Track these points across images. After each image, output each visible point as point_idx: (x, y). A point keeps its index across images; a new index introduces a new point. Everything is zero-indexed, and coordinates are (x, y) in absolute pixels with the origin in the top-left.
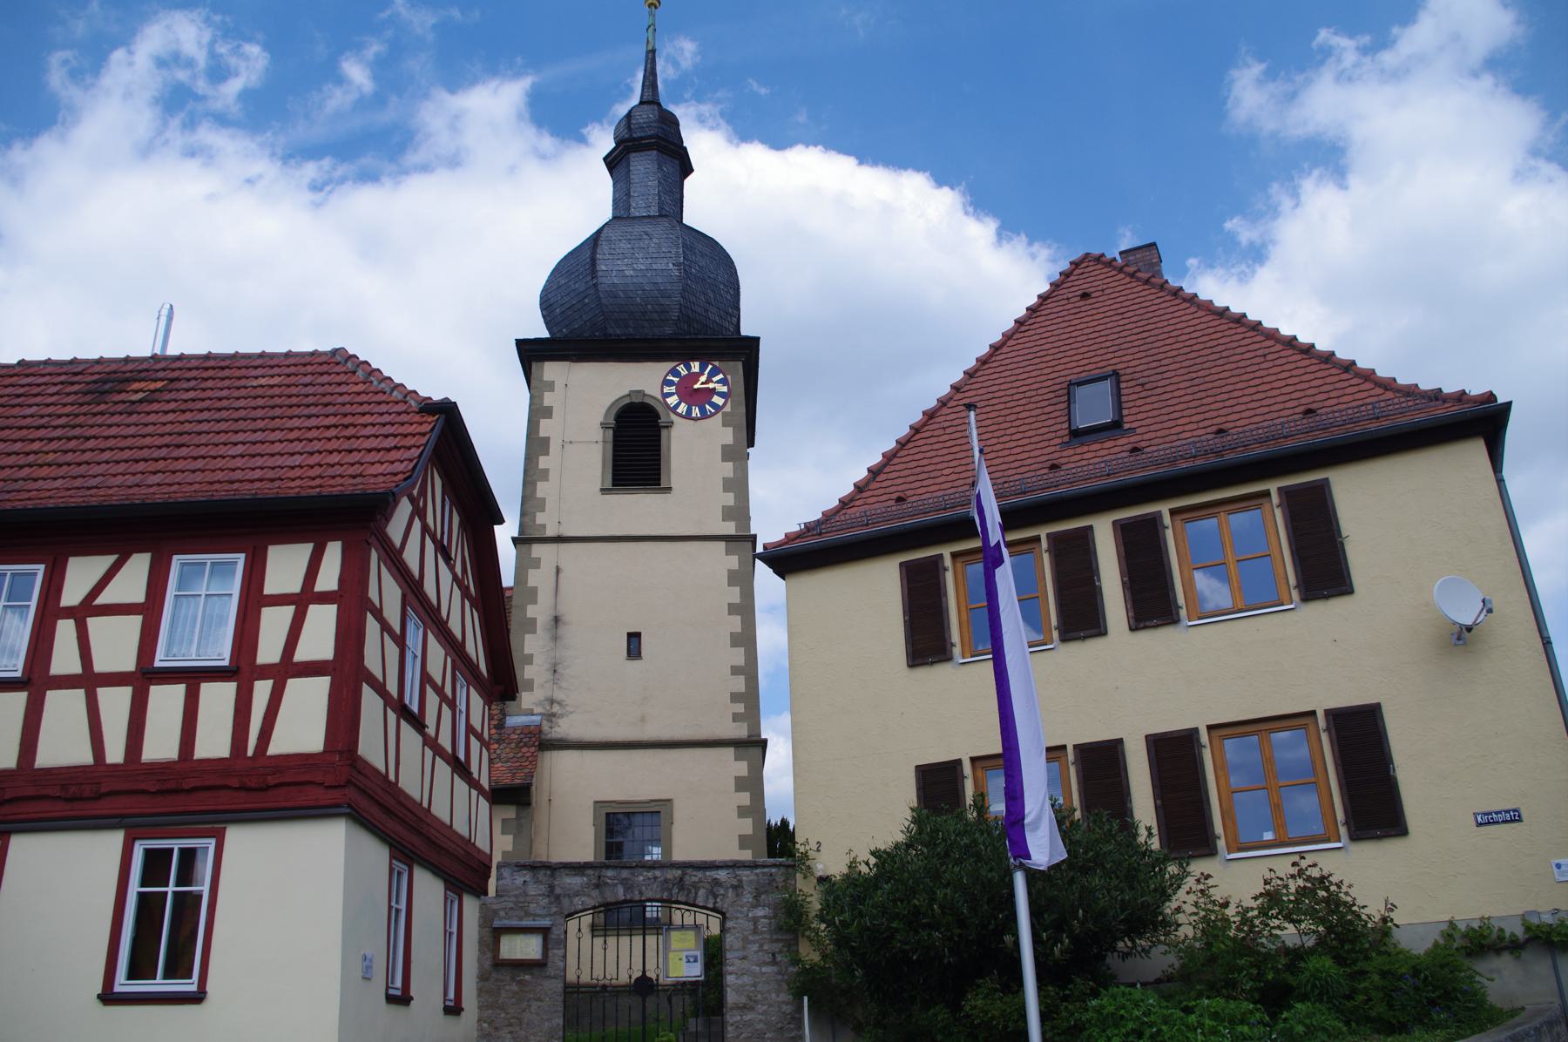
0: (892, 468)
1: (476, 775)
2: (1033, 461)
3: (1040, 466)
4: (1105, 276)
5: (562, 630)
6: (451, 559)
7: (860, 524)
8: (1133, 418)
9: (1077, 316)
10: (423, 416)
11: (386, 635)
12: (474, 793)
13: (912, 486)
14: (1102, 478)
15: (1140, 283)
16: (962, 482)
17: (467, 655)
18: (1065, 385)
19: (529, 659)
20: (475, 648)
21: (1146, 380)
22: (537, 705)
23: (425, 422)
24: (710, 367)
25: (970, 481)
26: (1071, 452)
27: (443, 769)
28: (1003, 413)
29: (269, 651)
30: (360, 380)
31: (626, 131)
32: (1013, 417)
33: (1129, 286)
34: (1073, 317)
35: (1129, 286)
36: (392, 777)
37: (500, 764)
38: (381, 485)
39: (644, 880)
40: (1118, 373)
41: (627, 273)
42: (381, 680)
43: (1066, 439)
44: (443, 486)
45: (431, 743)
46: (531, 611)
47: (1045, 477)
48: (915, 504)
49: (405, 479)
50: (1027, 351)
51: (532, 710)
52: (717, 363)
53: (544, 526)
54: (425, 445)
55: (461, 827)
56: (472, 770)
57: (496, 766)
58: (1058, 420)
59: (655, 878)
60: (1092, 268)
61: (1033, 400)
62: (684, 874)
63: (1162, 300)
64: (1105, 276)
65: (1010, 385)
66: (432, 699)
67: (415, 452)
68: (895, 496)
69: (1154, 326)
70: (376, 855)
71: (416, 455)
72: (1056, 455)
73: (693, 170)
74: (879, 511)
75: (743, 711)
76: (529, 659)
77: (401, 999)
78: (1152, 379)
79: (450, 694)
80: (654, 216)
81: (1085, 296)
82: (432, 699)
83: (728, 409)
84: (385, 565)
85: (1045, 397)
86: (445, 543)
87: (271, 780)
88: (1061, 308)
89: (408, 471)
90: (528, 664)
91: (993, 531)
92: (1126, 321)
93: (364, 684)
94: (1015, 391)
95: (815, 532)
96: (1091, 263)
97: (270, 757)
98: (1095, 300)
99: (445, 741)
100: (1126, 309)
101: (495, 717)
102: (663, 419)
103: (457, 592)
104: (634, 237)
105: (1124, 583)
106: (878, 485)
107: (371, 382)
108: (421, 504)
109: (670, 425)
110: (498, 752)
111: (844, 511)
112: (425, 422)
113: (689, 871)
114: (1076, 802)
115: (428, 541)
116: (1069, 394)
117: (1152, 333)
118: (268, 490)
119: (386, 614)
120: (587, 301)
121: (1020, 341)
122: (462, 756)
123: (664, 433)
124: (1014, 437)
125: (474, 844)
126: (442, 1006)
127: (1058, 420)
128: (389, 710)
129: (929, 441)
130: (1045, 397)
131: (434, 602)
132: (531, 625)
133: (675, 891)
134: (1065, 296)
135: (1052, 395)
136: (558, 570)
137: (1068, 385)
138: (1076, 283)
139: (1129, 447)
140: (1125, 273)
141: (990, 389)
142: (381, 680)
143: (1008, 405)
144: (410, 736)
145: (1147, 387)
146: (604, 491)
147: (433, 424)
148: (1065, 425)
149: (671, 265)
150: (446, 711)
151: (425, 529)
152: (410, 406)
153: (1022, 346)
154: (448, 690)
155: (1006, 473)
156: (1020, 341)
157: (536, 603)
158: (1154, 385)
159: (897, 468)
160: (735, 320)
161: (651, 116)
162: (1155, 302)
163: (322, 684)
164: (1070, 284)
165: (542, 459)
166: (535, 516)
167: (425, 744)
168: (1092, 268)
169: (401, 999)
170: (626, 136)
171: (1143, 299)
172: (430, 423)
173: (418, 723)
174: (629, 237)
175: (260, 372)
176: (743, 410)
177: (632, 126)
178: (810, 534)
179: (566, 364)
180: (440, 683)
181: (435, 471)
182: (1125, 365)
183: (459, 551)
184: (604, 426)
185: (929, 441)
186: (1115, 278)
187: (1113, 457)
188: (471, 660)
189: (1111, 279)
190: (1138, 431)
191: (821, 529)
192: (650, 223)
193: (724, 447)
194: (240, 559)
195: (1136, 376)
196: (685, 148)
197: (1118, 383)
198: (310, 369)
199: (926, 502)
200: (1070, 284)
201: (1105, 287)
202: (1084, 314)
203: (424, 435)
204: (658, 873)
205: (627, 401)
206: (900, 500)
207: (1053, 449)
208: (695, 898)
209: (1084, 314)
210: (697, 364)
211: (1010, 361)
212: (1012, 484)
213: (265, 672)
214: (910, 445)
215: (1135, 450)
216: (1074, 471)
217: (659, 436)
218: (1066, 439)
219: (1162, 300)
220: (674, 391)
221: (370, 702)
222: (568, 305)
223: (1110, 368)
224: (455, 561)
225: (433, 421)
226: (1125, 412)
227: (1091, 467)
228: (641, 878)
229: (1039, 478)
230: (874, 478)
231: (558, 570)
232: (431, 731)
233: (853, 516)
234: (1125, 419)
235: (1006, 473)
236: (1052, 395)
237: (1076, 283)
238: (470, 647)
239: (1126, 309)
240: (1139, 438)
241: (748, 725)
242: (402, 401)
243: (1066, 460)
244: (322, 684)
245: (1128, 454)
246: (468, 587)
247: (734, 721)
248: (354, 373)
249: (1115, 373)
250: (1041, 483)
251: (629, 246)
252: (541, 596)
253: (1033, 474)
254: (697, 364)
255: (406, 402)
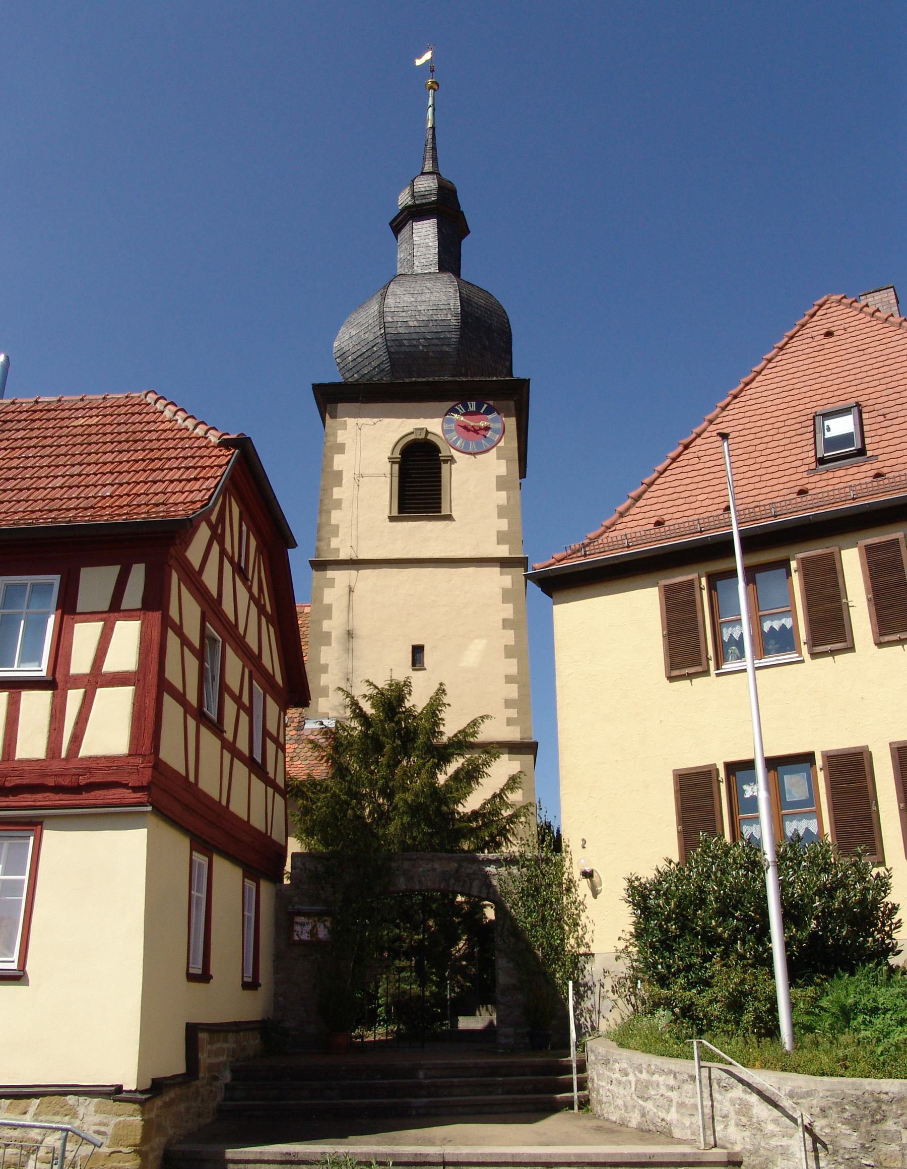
0: (651, 495)
1: (271, 775)
2: (781, 486)
3: (789, 491)
4: (846, 316)
5: (356, 643)
6: (248, 579)
7: (621, 546)
8: (876, 446)
9: (821, 353)
10: (221, 451)
11: (186, 649)
12: (270, 791)
13: (670, 510)
14: (847, 502)
15: (879, 322)
16: (716, 507)
17: (264, 666)
18: (811, 416)
19: (324, 669)
20: (271, 661)
21: (888, 410)
22: (332, 710)
23: (223, 455)
24: (485, 406)
25: (724, 506)
26: (816, 478)
27: (241, 770)
28: (753, 443)
29: (80, 663)
30: (167, 419)
31: (410, 198)
32: (763, 446)
33: (868, 325)
34: (817, 354)
35: (868, 325)
36: (192, 778)
37: (299, 762)
38: (180, 512)
39: (423, 871)
40: (860, 405)
41: (411, 324)
42: (181, 690)
43: (813, 466)
44: (241, 513)
45: (229, 747)
46: (326, 625)
47: (794, 501)
48: (672, 528)
49: (202, 507)
50: (775, 386)
51: (328, 714)
52: (491, 403)
53: (338, 550)
54: (222, 476)
55: (257, 822)
56: (268, 770)
57: (295, 763)
58: (805, 449)
59: (434, 870)
60: (835, 309)
61: (781, 430)
62: (460, 866)
63: (901, 336)
64: (846, 316)
65: (760, 395)
66: (230, 707)
67: (211, 483)
68: (654, 520)
69: (893, 361)
70: (180, 844)
71: (213, 486)
72: (806, 481)
73: (469, 232)
74: (638, 534)
75: (516, 716)
76: (324, 669)
77: (204, 977)
78: (892, 409)
79: (247, 703)
80: (434, 273)
81: (829, 334)
82: (230, 707)
83: (502, 444)
84: (185, 585)
85: (792, 428)
86: (243, 565)
87: (83, 781)
88: (806, 346)
89: (206, 500)
90: (324, 673)
91: (235, 1152)
92: (868, 357)
93: (165, 693)
94: (764, 422)
95: (579, 554)
96: (833, 305)
97: (82, 759)
98: (837, 338)
99: (242, 745)
100: (867, 346)
101: (295, 720)
102: (443, 453)
103: (254, 610)
104: (416, 292)
105: (869, 600)
106: (638, 510)
107: (177, 420)
108: (219, 531)
109: (451, 460)
110: (298, 750)
111: (606, 535)
112: (223, 455)
113: (465, 864)
114: (827, 828)
115: (226, 563)
116: (814, 424)
117: (892, 367)
118: (84, 518)
119: (186, 630)
120: (375, 349)
121: (768, 377)
122: (258, 757)
123: (445, 467)
124: (764, 465)
125: (271, 836)
126: (241, 982)
127: (805, 449)
128: (189, 718)
129: (685, 469)
130: (792, 428)
131: (232, 619)
132: (326, 639)
133: (452, 881)
134: (809, 335)
135: (799, 426)
136: (351, 590)
137: (814, 417)
138: (819, 323)
139: (873, 473)
140: (865, 313)
141: (741, 421)
142: (181, 690)
143: (759, 435)
144: (209, 741)
145: (888, 417)
146: (392, 519)
147: (230, 457)
148: (812, 453)
149: (449, 315)
150: (244, 718)
151: (223, 552)
152: (210, 441)
153: (770, 381)
154: (245, 699)
155: (757, 498)
156: (768, 377)
157: (330, 618)
158: (895, 415)
159: (655, 494)
160: (508, 364)
161: (432, 184)
162: (893, 339)
163: (127, 693)
164: (815, 324)
165: (335, 490)
166: (330, 541)
167: (223, 747)
168: (835, 309)
169: (204, 977)
170: (410, 203)
171: (882, 336)
172: (227, 456)
173: (217, 728)
174: (412, 292)
175: (80, 413)
176: (515, 444)
177: (415, 194)
178: (574, 555)
179: (358, 405)
180: (237, 693)
181: (233, 500)
182: (867, 397)
183: (257, 573)
184: (392, 461)
185: (685, 469)
186: (856, 318)
187: (857, 482)
188: (267, 670)
189: (852, 319)
190: (880, 458)
191: (585, 551)
192: (431, 279)
193: (498, 477)
194: (56, 579)
195: (877, 407)
196: (462, 212)
197: (860, 413)
198: (123, 410)
199: (682, 526)
200: (815, 324)
201: (847, 326)
202: (828, 351)
203: (220, 466)
204: (437, 866)
205: (412, 437)
206: (659, 524)
207: (800, 476)
208: (470, 888)
209: (828, 351)
210: (474, 403)
211: (760, 395)
212: (762, 508)
213: (76, 681)
214: (667, 473)
215: (878, 475)
216: (820, 496)
217: (440, 468)
218: (813, 466)
219: (901, 336)
220: (453, 428)
221: (172, 710)
222: (359, 353)
223: (855, 400)
224: (252, 582)
225: (229, 455)
226: (867, 441)
227: (836, 492)
228: (421, 869)
229: (788, 502)
230: (634, 504)
231: (351, 590)
232: (229, 736)
233: (614, 539)
234: (868, 447)
235: (757, 498)
236: (799, 426)
237: (819, 323)
238: (266, 661)
239: (867, 346)
240: (881, 465)
241: (521, 728)
242: (202, 437)
243: (813, 486)
244: (127, 693)
245: (871, 479)
246: (265, 605)
247: (508, 725)
248: (162, 412)
249: (858, 405)
250: (789, 507)
251: (413, 299)
252: (335, 612)
253: (781, 499)
254: (474, 403)
255: (206, 438)
